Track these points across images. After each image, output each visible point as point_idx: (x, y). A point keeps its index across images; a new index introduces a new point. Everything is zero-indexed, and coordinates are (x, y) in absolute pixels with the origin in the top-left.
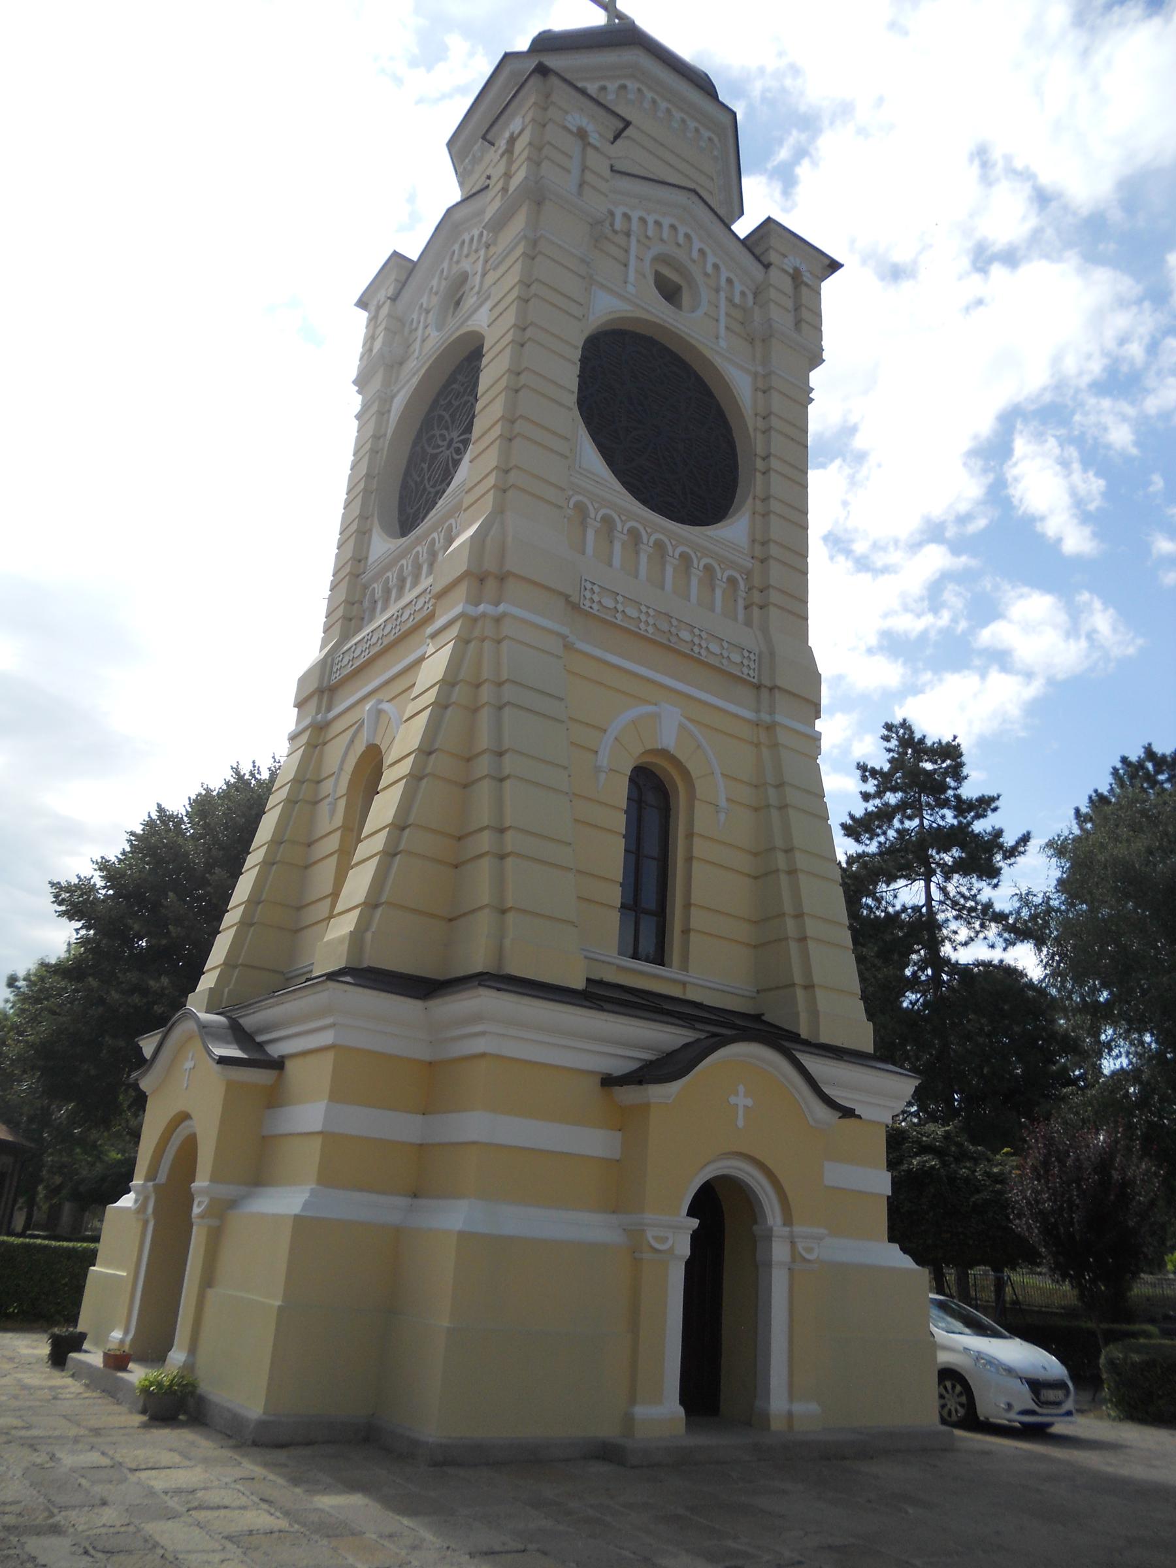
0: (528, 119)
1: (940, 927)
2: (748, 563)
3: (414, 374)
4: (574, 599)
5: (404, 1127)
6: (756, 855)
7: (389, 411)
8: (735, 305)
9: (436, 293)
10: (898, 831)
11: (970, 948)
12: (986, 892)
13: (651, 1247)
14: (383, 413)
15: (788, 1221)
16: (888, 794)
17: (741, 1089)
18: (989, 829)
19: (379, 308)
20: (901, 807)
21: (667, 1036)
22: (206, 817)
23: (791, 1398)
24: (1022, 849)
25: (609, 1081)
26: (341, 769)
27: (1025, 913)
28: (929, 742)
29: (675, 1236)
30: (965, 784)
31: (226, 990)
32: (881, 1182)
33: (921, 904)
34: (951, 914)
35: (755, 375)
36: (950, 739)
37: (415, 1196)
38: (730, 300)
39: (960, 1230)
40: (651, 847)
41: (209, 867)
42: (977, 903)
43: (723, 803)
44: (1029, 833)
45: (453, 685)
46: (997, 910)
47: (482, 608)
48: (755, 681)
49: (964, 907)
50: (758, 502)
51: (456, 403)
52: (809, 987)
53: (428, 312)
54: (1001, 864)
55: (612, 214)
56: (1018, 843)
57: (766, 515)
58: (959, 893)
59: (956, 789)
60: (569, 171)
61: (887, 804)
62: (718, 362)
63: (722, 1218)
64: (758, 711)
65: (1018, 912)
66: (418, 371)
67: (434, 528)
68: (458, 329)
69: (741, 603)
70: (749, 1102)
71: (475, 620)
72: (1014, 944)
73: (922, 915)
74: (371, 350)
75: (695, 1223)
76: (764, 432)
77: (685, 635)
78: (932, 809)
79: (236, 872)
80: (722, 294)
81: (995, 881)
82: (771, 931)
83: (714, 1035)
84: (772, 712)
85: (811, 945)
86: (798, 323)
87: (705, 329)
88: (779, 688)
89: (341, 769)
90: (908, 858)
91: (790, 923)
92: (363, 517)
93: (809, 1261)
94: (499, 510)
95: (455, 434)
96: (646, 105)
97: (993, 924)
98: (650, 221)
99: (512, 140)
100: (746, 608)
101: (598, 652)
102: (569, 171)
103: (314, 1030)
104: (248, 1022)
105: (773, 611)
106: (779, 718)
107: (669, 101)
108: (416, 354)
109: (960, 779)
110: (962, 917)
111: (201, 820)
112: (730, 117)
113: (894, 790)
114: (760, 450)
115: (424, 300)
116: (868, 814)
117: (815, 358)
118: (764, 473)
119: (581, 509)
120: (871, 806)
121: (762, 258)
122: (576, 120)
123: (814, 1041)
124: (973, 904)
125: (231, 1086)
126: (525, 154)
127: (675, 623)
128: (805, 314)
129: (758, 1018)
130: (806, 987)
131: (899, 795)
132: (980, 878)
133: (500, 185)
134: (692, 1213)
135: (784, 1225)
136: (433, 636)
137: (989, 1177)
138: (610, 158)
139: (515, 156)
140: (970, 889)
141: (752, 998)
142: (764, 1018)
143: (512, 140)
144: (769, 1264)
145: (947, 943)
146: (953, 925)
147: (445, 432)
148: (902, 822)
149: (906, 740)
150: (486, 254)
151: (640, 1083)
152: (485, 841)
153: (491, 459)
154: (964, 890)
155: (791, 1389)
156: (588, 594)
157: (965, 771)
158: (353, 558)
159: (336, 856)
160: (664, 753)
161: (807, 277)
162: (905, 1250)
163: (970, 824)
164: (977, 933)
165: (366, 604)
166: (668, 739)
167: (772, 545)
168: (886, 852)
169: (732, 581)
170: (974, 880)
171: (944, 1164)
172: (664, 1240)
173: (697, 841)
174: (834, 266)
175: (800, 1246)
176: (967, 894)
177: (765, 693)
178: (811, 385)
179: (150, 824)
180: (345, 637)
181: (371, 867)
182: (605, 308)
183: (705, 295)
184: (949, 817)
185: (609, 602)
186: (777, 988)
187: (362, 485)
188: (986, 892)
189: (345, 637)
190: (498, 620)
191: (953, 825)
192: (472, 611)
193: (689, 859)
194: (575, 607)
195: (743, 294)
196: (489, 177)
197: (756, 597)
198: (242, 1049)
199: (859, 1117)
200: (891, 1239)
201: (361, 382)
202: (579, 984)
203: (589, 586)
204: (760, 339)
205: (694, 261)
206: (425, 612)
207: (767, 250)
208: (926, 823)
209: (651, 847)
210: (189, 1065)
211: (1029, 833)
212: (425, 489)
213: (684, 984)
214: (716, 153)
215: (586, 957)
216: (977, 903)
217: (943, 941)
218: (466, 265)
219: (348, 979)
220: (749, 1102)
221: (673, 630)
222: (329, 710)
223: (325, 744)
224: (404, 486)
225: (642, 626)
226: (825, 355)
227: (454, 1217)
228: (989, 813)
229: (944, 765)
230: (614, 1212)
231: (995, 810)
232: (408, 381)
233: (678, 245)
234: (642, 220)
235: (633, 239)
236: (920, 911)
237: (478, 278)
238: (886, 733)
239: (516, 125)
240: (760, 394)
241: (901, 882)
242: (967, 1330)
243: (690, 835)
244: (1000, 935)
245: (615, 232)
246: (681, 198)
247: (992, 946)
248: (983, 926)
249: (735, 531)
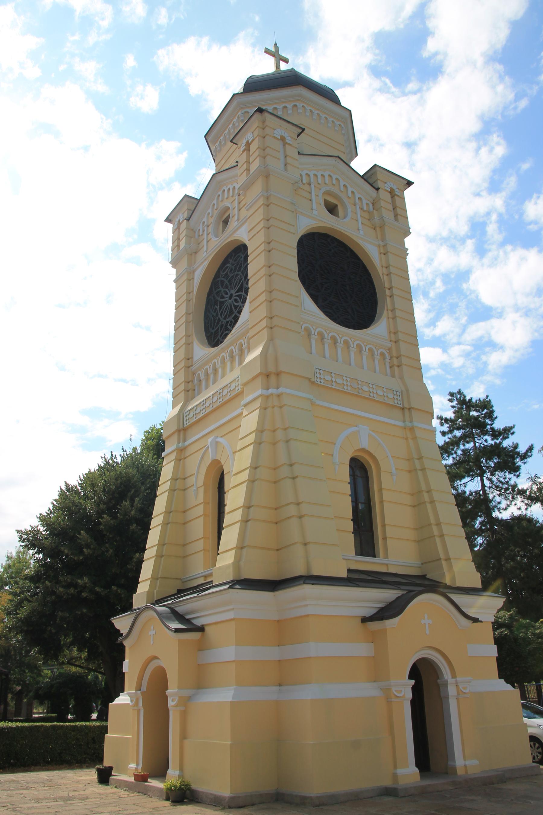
0: (256, 134)
1: (491, 501)
2: (389, 345)
3: (206, 259)
4: (313, 380)
5: (271, 653)
6: (412, 495)
7: (193, 278)
8: (364, 211)
9: (212, 217)
10: (463, 451)
11: (508, 510)
12: (513, 479)
13: (395, 695)
14: (190, 280)
15: (454, 676)
16: (455, 431)
17: (426, 616)
18: (511, 444)
19: (179, 224)
20: (463, 438)
21: (388, 595)
22: (94, 487)
23: (465, 760)
24: (529, 454)
25: (365, 620)
26: (198, 472)
27: (535, 488)
28: (474, 401)
29: (405, 689)
30: (496, 421)
31: (155, 591)
32: (493, 651)
33: (479, 489)
34: (496, 493)
35: (379, 246)
36: (485, 397)
37: (280, 685)
38: (362, 209)
39: (523, 665)
40: (362, 498)
41: (100, 513)
42: (509, 486)
43: (394, 471)
44: (532, 445)
45: (262, 432)
46: (520, 488)
47: (271, 391)
48: (401, 406)
49: (502, 488)
50: (390, 312)
51: (231, 275)
52: (448, 559)
53: (208, 226)
54: (520, 463)
55: (301, 175)
56: (527, 451)
57: (394, 318)
58: (499, 481)
59: (491, 425)
60: (279, 159)
61: (455, 437)
62: (360, 242)
63: (424, 677)
64: (404, 421)
65: (531, 488)
66: (207, 258)
67: (231, 344)
68: (228, 238)
69: (388, 366)
70: (430, 622)
71: (268, 397)
72: (531, 506)
73: (480, 495)
74: (178, 246)
75: (413, 682)
76: (387, 275)
77: (366, 388)
78: (479, 436)
79: (146, 528)
80: (358, 207)
81: (518, 473)
82: (425, 534)
83: (410, 591)
84: (411, 421)
85: (446, 538)
86: (396, 216)
87: (352, 228)
88: (413, 408)
89: (198, 472)
90: (469, 466)
91: (435, 528)
92: (187, 336)
93: (465, 693)
94: (271, 339)
95: (233, 292)
96: (308, 114)
97: (518, 496)
98: (319, 175)
99: (248, 144)
100: (391, 367)
101: (326, 405)
102: (279, 159)
103: (219, 610)
104: (180, 609)
105: (404, 368)
106: (415, 424)
107: (318, 110)
108: (205, 249)
109: (492, 419)
110: (502, 495)
111: (91, 489)
112: (348, 113)
113: (458, 429)
114: (387, 285)
115: (205, 220)
116: (446, 443)
117: (407, 232)
118: (390, 297)
119: (307, 330)
120: (446, 439)
121: (373, 185)
122: (278, 133)
123: (454, 586)
124: (506, 486)
125: (180, 642)
126: (257, 153)
127: (360, 382)
128: (399, 211)
129: (423, 577)
130: (446, 560)
131: (461, 431)
132: (510, 473)
133: (245, 167)
134: (410, 677)
135: (452, 678)
136: (245, 405)
137: (534, 636)
138: (297, 148)
139: (251, 153)
140: (505, 479)
141: (420, 567)
142: (427, 577)
143: (248, 144)
144: (447, 697)
145: (496, 510)
146: (498, 499)
147: (226, 290)
148: (464, 445)
149: (463, 404)
150: (239, 199)
151: (382, 619)
152: (292, 510)
153: (262, 312)
154: (501, 479)
155: (466, 757)
156: (318, 375)
157: (495, 415)
158: (185, 358)
159: (203, 517)
160: (363, 450)
161: (397, 192)
162: (507, 681)
163: (501, 443)
164: (511, 502)
165: (196, 382)
166: (365, 444)
167: (399, 334)
168: (458, 464)
169: (382, 354)
170: (507, 474)
171: (511, 632)
172: (400, 691)
173: (384, 492)
174: (409, 183)
175: (461, 687)
176: (503, 481)
177: (406, 411)
178: (406, 247)
179: (62, 494)
180: (187, 401)
181: (236, 528)
182: (306, 224)
183: (350, 208)
184: (489, 440)
185: (328, 378)
186: (432, 561)
187: (184, 319)
188: (513, 479)
189: (187, 401)
190: (278, 396)
191: (492, 445)
192: (265, 392)
193: (382, 502)
194: (313, 383)
195: (367, 204)
196: (237, 162)
197: (395, 361)
198: (181, 623)
199: (481, 622)
200: (500, 678)
201: (174, 263)
202: (344, 575)
203: (318, 371)
204: (379, 228)
205: (342, 192)
206: (237, 391)
207: (377, 180)
208: (477, 444)
209: (362, 498)
210: (152, 633)
211: (532, 445)
212: (219, 320)
213: (387, 565)
214: (343, 132)
215: (343, 559)
216: (509, 486)
217: (493, 509)
218: (227, 203)
219: (237, 586)
220: (430, 622)
221: (359, 387)
222: (185, 441)
223: (185, 458)
224: (206, 317)
225: (345, 387)
226: (411, 230)
227: (307, 693)
228: (510, 435)
229: (484, 412)
230: (375, 681)
231: (513, 433)
232: (202, 263)
233: (333, 185)
234: (315, 175)
235: (312, 186)
236: (479, 493)
237: (236, 210)
238: (450, 398)
239: (249, 137)
240: (382, 255)
241: (466, 479)
242: (537, 716)
243: (380, 490)
244: (523, 501)
245: (304, 184)
246: (332, 161)
247: (520, 509)
248: (513, 498)
249: (379, 329)
